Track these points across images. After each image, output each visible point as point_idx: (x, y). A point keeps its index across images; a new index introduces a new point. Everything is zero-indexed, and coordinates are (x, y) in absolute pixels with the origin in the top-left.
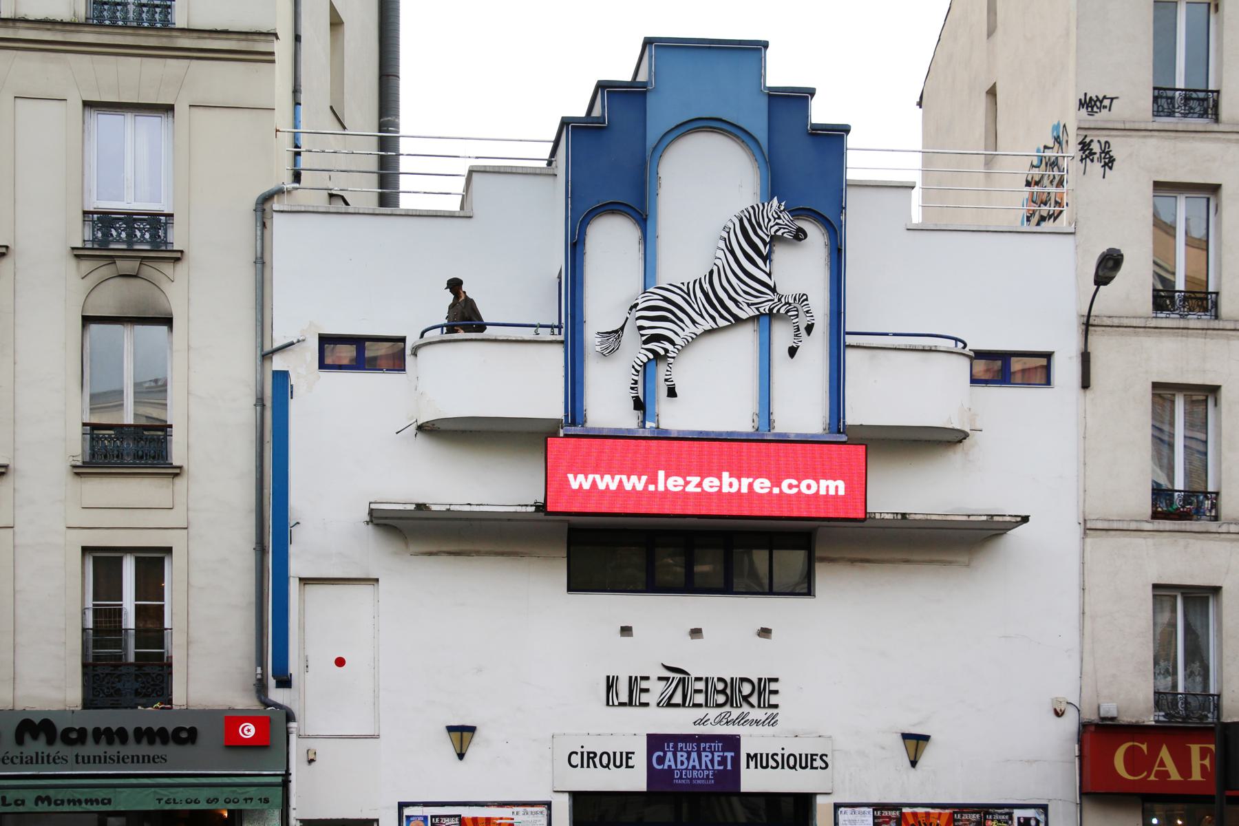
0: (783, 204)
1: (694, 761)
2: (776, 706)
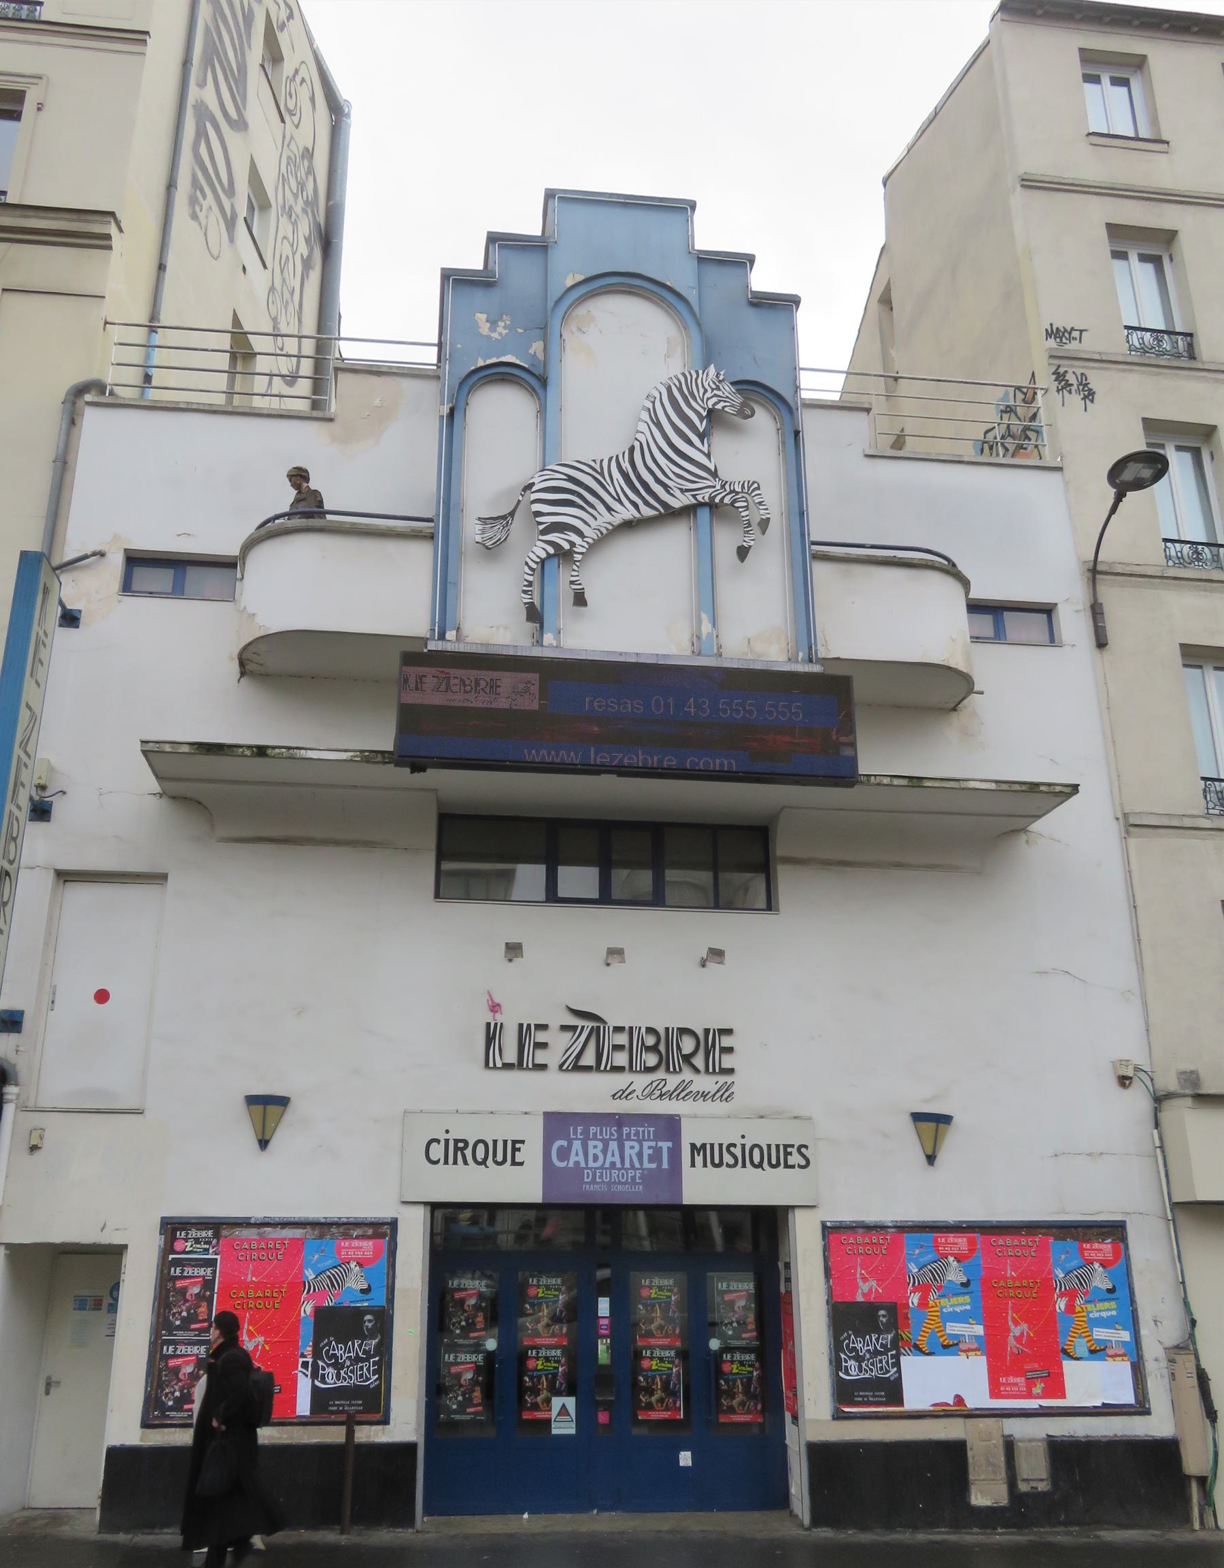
0: (722, 373)
1: (613, 1155)
2: (731, 1071)
